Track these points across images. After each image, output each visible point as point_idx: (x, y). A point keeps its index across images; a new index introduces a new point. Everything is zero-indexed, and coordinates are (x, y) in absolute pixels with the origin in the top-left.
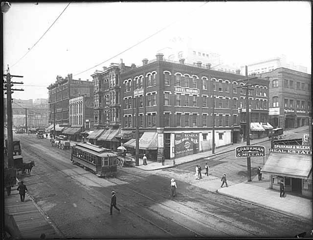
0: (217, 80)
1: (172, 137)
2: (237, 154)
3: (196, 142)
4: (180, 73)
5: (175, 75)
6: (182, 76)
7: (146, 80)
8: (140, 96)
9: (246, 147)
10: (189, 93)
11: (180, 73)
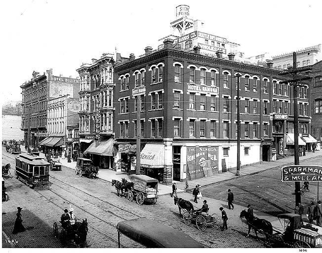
0: (209, 69)
1: (183, 151)
2: (284, 177)
3: (215, 158)
4: (180, 64)
5: (188, 67)
6: (197, 69)
7: (148, 74)
8: (285, 101)
9: (293, 168)
10: (206, 93)
11: (180, 64)
